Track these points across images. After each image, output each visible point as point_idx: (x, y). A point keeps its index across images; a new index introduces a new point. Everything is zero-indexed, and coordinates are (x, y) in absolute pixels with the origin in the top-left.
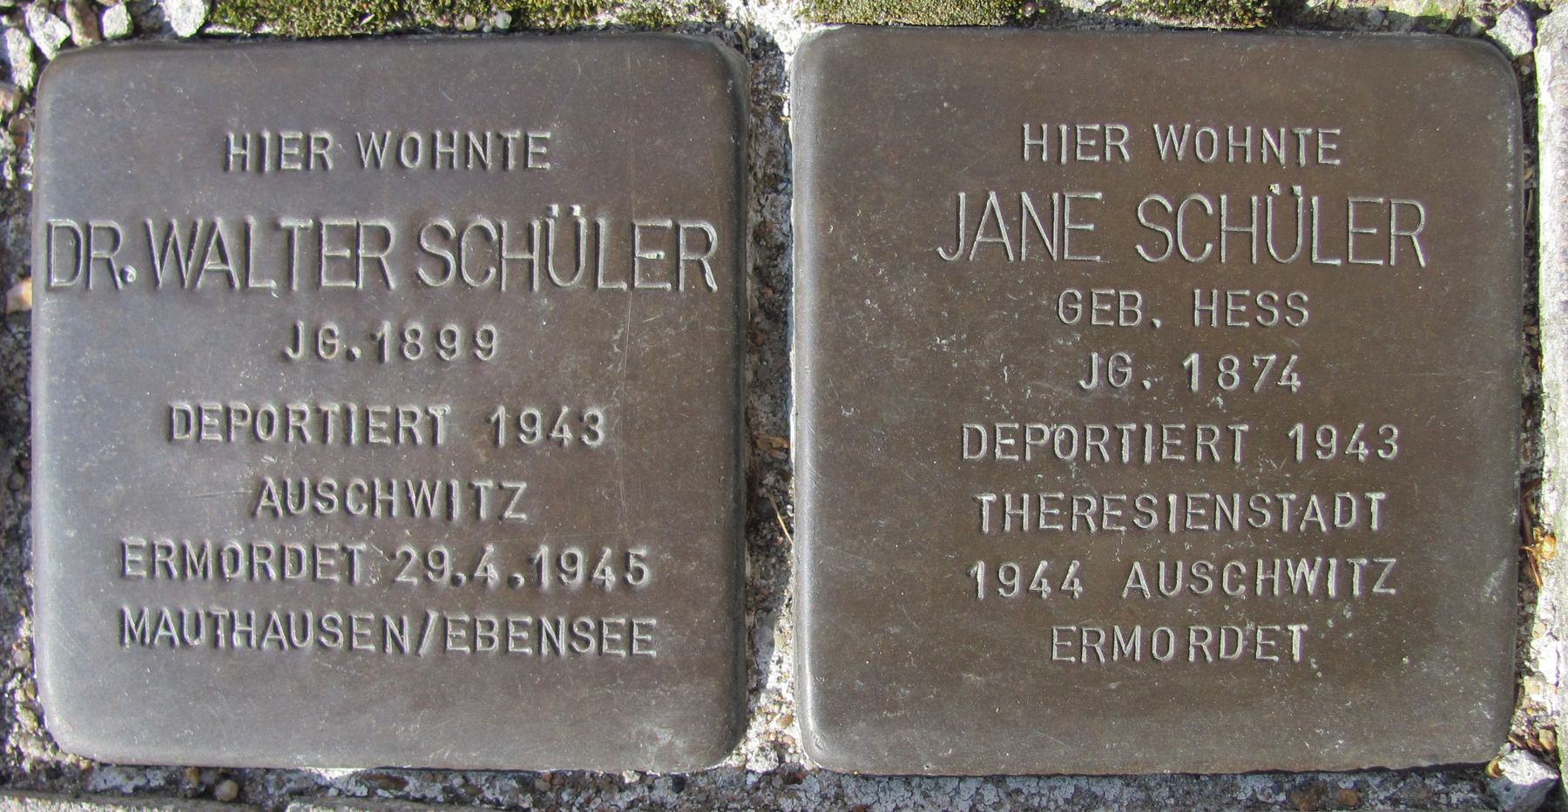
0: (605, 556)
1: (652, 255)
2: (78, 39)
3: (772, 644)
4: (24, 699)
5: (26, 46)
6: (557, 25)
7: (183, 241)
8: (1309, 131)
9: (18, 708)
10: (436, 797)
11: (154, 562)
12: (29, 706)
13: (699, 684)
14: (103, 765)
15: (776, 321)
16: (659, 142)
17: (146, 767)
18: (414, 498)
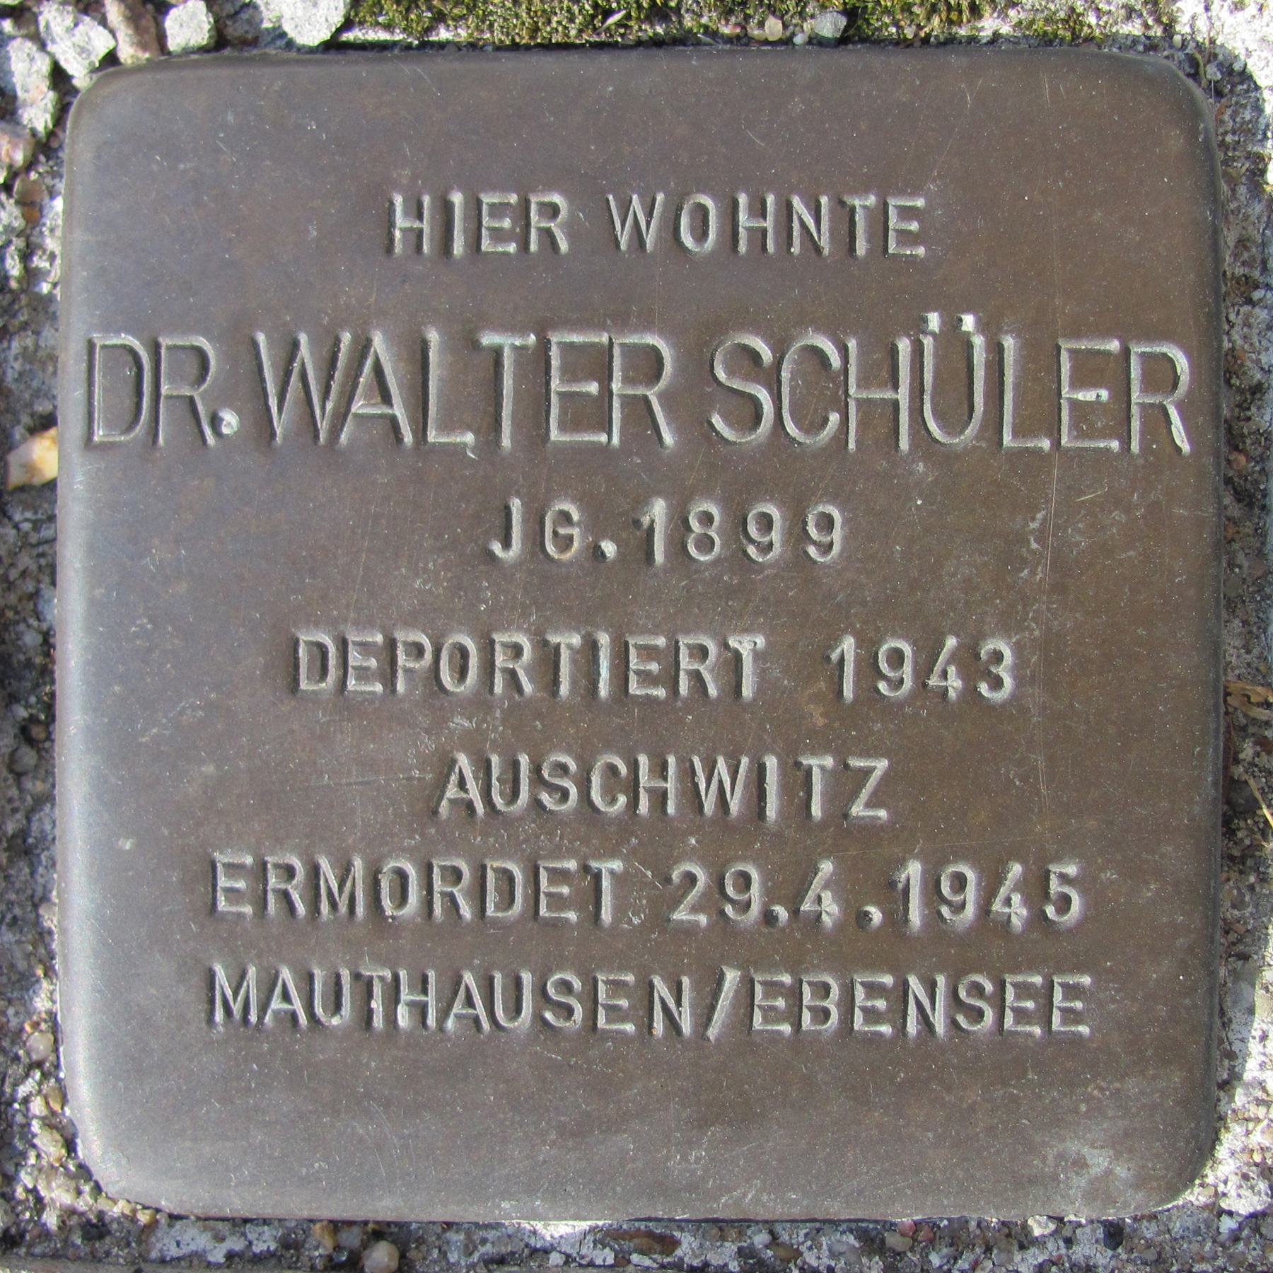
0: (1010, 875)
1: (1087, 396)
2: (127, 53)
3: (1251, 1011)
4: (45, 1112)
5: (43, 65)
6: (916, 35)
7: (316, 368)
8: (871, 200)
9: (36, 1126)
10: (726, 1265)
11: (265, 892)
12: (52, 1122)
13: (1154, 1078)
14: (174, 1218)
15: (1250, 505)
16: (1098, 216)
17: (246, 1221)
18: (702, 786)
